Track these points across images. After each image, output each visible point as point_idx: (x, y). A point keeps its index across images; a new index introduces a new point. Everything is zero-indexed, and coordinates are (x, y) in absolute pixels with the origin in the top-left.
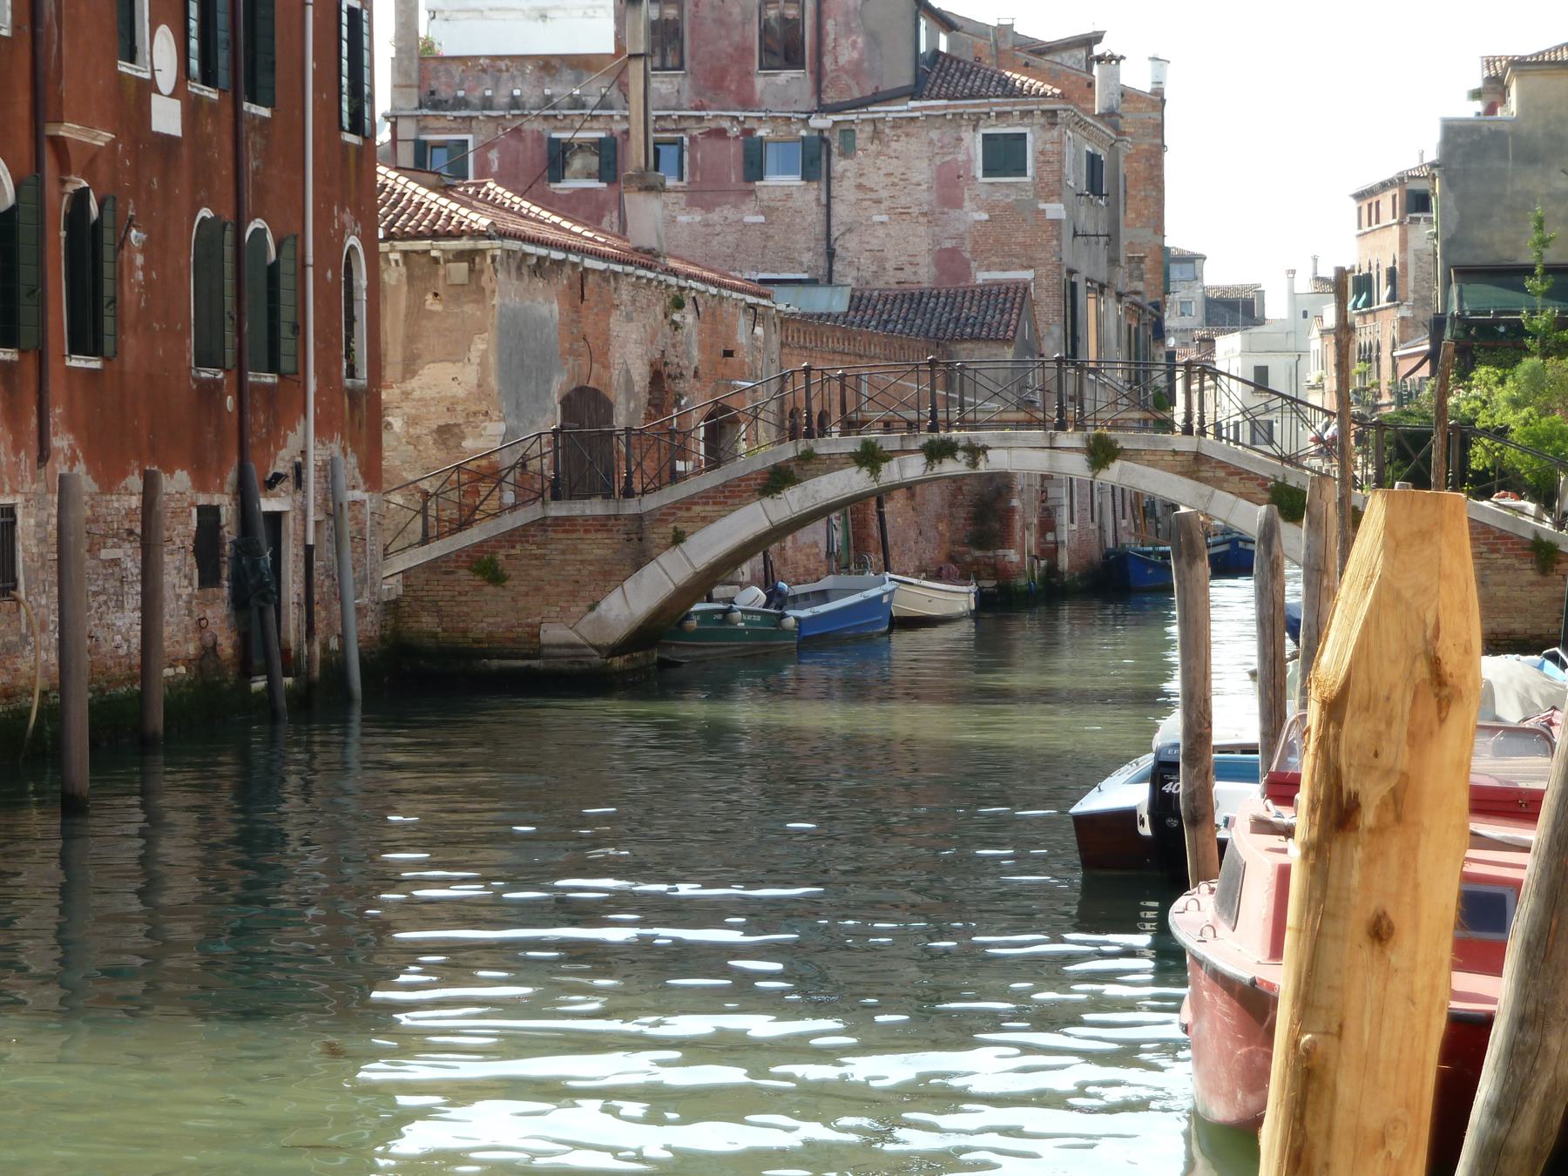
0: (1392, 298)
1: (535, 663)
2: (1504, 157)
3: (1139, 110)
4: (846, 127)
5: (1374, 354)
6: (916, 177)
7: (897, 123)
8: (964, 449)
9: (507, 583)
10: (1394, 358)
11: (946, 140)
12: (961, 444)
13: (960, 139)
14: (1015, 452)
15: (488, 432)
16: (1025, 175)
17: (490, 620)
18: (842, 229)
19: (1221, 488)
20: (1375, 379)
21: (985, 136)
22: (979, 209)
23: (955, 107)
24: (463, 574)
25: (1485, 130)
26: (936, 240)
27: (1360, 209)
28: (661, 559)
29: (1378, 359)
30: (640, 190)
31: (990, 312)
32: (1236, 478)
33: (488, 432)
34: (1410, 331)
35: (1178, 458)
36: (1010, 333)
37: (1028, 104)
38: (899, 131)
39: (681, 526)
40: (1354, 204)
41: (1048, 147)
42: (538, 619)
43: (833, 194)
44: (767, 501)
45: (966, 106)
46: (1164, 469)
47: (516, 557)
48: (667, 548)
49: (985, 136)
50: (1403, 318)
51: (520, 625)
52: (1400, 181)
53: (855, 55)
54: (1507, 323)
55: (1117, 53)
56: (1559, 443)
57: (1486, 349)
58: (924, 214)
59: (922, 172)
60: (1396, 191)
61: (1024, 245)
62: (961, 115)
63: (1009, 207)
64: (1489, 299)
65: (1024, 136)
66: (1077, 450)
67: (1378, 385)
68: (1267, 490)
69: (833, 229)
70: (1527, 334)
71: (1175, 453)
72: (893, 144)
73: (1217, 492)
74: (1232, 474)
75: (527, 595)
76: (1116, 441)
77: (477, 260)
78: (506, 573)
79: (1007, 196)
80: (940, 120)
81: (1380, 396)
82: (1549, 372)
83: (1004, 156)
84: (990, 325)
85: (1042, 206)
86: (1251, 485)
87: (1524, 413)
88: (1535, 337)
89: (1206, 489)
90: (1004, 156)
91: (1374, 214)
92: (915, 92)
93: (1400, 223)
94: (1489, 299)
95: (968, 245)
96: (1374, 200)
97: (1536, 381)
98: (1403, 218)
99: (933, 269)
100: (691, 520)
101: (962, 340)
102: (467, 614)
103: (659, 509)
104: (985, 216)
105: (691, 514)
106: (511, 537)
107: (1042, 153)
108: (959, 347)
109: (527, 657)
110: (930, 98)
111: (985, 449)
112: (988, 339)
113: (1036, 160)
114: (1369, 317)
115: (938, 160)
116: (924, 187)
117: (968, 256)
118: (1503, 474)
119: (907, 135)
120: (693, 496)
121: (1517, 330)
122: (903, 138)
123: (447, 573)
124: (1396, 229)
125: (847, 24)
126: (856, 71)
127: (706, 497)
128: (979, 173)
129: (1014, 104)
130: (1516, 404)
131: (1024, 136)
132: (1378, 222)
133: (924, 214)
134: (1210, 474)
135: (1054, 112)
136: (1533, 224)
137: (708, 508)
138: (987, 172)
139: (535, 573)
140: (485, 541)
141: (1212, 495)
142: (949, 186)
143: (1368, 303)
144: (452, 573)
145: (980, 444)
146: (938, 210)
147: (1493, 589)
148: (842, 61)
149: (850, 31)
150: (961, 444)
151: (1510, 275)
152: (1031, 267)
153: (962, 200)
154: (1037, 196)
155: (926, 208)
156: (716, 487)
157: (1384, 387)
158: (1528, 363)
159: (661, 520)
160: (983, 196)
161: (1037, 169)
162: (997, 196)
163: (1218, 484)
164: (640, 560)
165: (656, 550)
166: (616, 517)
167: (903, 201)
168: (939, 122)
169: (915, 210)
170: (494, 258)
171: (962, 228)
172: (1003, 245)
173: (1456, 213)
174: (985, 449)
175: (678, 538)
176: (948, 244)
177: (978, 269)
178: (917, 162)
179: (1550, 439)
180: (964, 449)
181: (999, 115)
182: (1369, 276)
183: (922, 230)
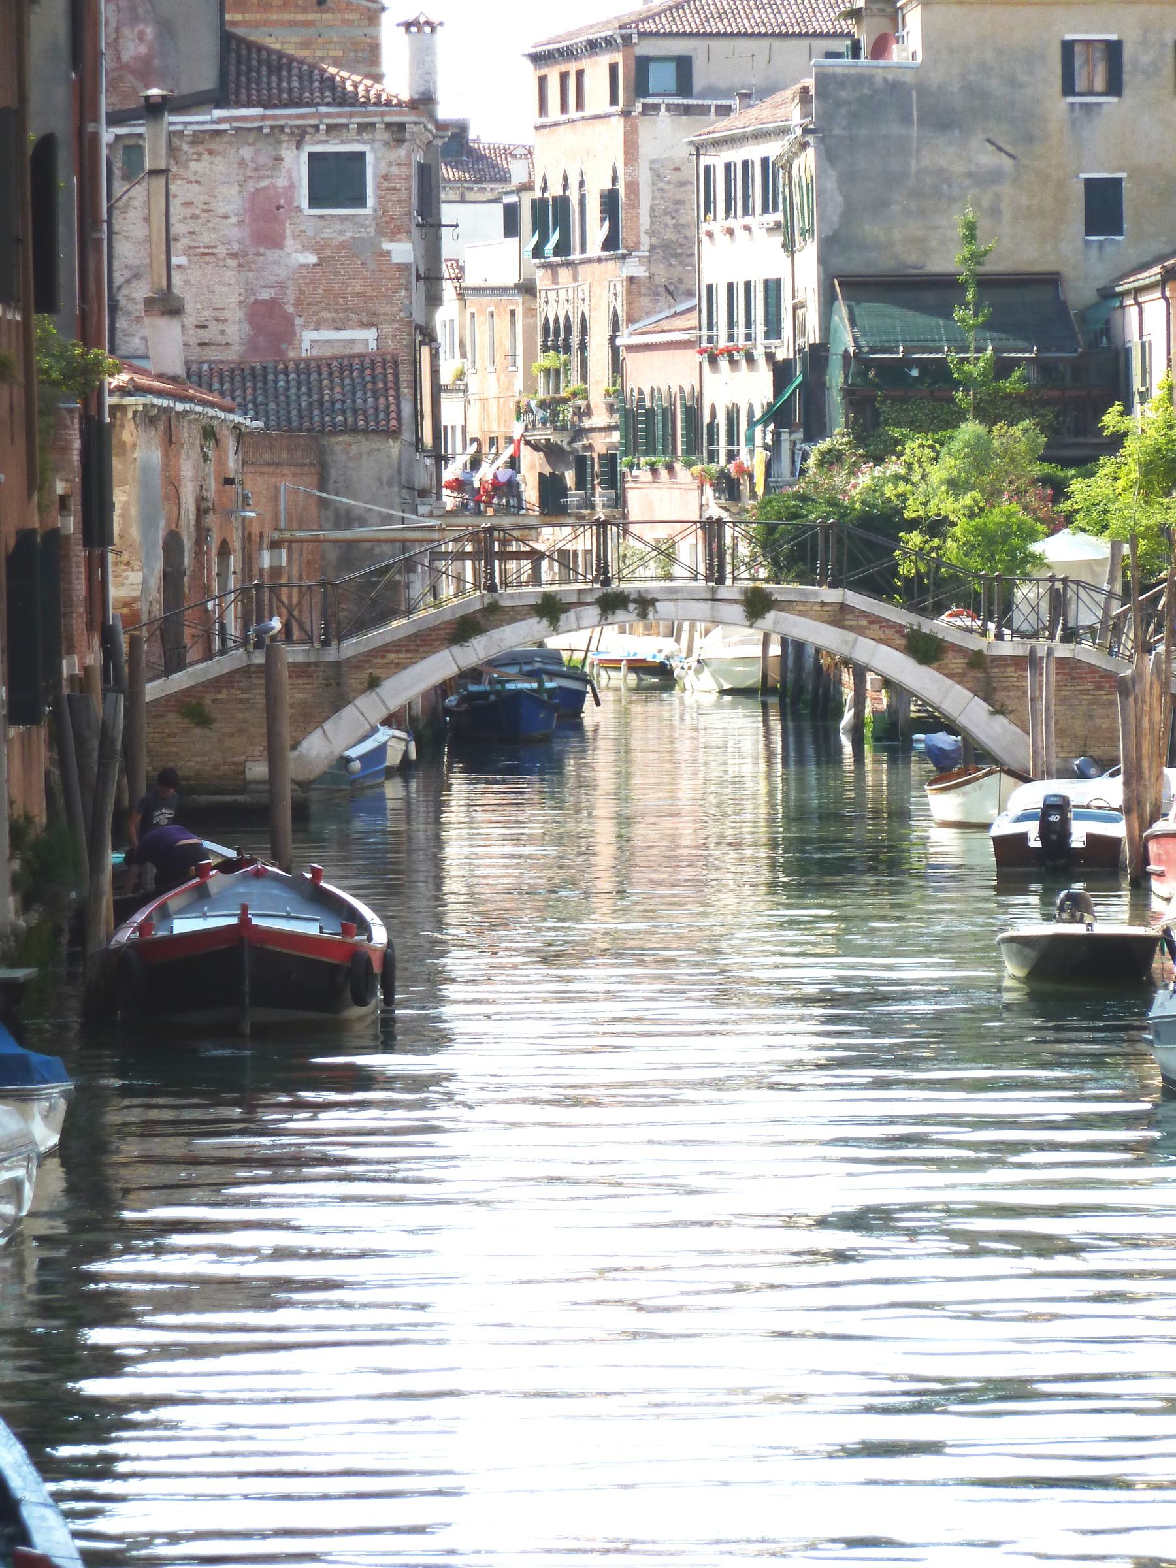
0: (611, 242)
1: (241, 798)
2: (906, 119)
3: (349, 23)
4: (131, 142)
5: (575, 339)
6: (222, 208)
7: (198, 138)
8: (635, 601)
9: (213, 726)
10: (615, 351)
11: (262, 159)
12: (632, 597)
13: (279, 159)
14: (681, 604)
15: (130, 581)
16: (364, 206)
17: (198, 759)
18: (128, 274)
19: (863, 635)
20: (576, 384)
21: (311, 155)
22: (305, 248)
23: (274, 117)
24: (172, 717)
25: (878, 80)
26: (250, 290)
27: (542, 80)
28: (358, 702)
29: (583, 346)
30: (163, 313)
31: (359, 394)
32: (877, 627)
33: (130, 581)
34: (645, 301)
35: (825, 608)
36: (393, 423)
37: (365, 115)
38: (201, 148)
39: (376, 672)
40: (530, 73)
41: (394, 170)
42: (243, 758)
43: (116, 228)
44: (456, 649)
45: (289, 117)
46: (813, 618)
47: (222, 701)
48: (363, 692)
49: (311, 155)
50: (631, 280)
51: (226, 764)
52: (625, 37)
53: (143, 49)
54: (920, 363)
55: (435, 19)
56: (1016, 541)
57: (894, 401)
58: (234, 256)
59: (230, 201)
60: (618, 57)
61: (363, 296)
62: (282, 128)
63: (344, 247)
64: (903, 331)
65: (362, 155)
66: (736, 601)
67: (584, 394)
68: (904, 636)
69: (116, 275)
70: (957, 384)
71: (823, 604)
72: (193, 165)
73: (860, 638)
74: (871, 622)
75: (232, 735)
76: (771, 594)
77: (118, 414)
78: (213, 716)
79: (342, 232)
80: (253, 135)
81: (588, 412)
82: (996, 443)
83: (336, 181)
84: (365, 411)
85: (386, 246)
86: (889, 633)
87: (967, 499)
88: (966, 391)
89: (851, 636)
90: (336, 181)
91: (573, 93)
92: (220, 97)
93: (626, 114)
94: (903, 331)
95: (291, 296)
96: (572, 67)
97: (980, 456)
98: (629, 103)
99: (246, 327)
100: (385, 666)
101: (334, 432)
102: (177, 754)
103: (355, 656)
104: (312, 259)
105: (384, 661)
106: (218, 683)
107: (386, 177)
108: (333, 440)
109: (233, 792)
110: (239, 105)
111: (653, 602)
112: (365, 431)
113: (378, 187)
114: (564, 274)
115: (251, 186)
116: (233, 220)
117: (291, 309)
118: (939, 583)
119: (211, 152)
120: (384, 646)
121: (938, 372)
122: (205, 157)
123: (156, 716)
124: (618, 124)
125: (133, 9)
126: (145, 72)
127: (399, 645)
128: (305, 203)
129: (351, 115)
130: (955, 486)
131: (362, 155)
132: (580, 105)
133: (234, 256)
134: (853, 623)
135: (402, 126)
136: (961, 231)
137: (402, 655)
138: (314, 202)
139: (240, 716)
140: (193, 687)
141: (856, 639)
142: (266, 221)
143: (563, 248)
144: (161, 716)
145: (650, 597)
146: (251, 250)
147: (1098, 721)
148: (126, 56)
149: (135, 19)
150: (632, 597)
151: (929, 291)
152: (372, 325)
153: (283, 237)
154: (380, 232)
155: (236, 247)
156: (409, 637)
157: (597, 398)
158: (970, 429)
159: (357, 667)
160: (310, 233)
161: (380, 198)
162: (328, 233)
163: (860, 631)
164: (338, 702)
165: (353, 694)
166: (316, 664)
167: (207, 238)
168: (251, 137)
169: (221, 250)
170: (135, 413)
171: (283, 273)
172: (336, 296)
173: (839, 199)
174: (653, 602)
175: (374, 683)
176: (265, 295)
177: (304, 326)
178: (224, 189)
179: (1006, 537)
180: (635, 601)
181: (330, 128)
182: (562, 203)
183: (230, 276)
